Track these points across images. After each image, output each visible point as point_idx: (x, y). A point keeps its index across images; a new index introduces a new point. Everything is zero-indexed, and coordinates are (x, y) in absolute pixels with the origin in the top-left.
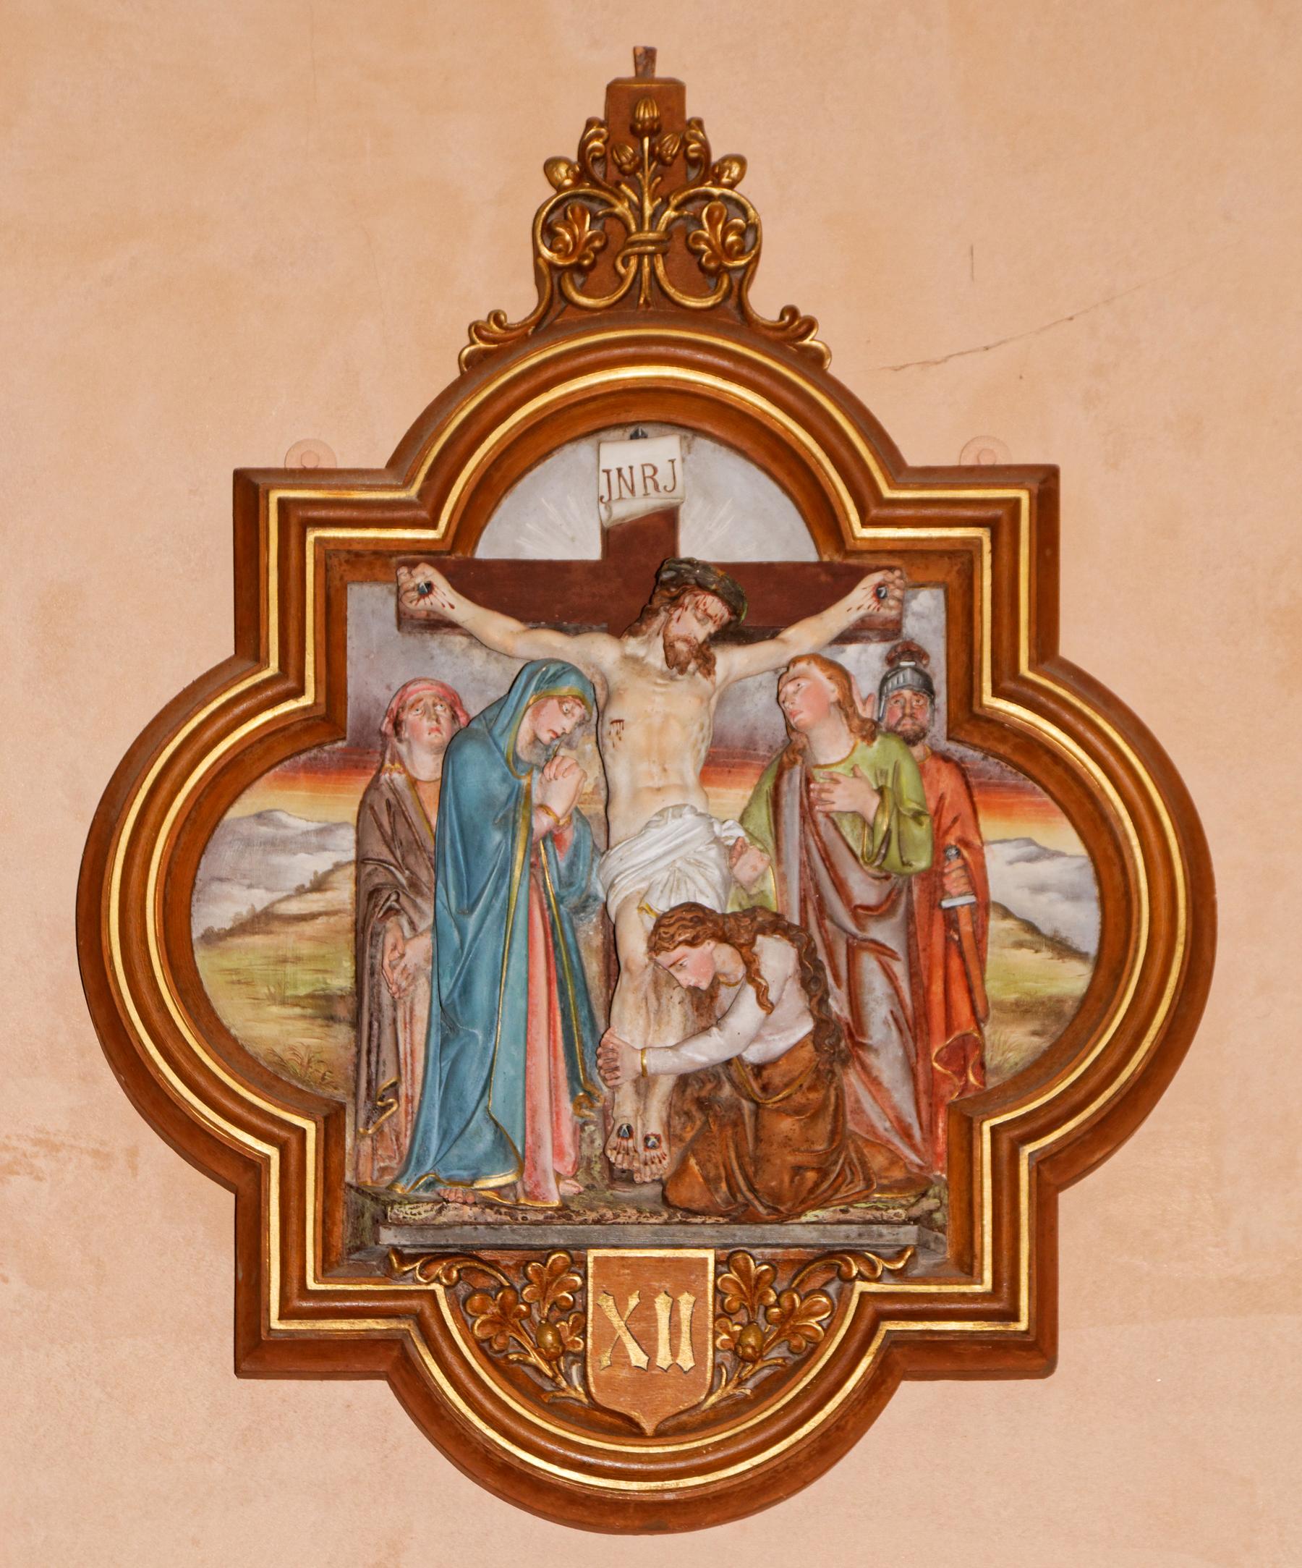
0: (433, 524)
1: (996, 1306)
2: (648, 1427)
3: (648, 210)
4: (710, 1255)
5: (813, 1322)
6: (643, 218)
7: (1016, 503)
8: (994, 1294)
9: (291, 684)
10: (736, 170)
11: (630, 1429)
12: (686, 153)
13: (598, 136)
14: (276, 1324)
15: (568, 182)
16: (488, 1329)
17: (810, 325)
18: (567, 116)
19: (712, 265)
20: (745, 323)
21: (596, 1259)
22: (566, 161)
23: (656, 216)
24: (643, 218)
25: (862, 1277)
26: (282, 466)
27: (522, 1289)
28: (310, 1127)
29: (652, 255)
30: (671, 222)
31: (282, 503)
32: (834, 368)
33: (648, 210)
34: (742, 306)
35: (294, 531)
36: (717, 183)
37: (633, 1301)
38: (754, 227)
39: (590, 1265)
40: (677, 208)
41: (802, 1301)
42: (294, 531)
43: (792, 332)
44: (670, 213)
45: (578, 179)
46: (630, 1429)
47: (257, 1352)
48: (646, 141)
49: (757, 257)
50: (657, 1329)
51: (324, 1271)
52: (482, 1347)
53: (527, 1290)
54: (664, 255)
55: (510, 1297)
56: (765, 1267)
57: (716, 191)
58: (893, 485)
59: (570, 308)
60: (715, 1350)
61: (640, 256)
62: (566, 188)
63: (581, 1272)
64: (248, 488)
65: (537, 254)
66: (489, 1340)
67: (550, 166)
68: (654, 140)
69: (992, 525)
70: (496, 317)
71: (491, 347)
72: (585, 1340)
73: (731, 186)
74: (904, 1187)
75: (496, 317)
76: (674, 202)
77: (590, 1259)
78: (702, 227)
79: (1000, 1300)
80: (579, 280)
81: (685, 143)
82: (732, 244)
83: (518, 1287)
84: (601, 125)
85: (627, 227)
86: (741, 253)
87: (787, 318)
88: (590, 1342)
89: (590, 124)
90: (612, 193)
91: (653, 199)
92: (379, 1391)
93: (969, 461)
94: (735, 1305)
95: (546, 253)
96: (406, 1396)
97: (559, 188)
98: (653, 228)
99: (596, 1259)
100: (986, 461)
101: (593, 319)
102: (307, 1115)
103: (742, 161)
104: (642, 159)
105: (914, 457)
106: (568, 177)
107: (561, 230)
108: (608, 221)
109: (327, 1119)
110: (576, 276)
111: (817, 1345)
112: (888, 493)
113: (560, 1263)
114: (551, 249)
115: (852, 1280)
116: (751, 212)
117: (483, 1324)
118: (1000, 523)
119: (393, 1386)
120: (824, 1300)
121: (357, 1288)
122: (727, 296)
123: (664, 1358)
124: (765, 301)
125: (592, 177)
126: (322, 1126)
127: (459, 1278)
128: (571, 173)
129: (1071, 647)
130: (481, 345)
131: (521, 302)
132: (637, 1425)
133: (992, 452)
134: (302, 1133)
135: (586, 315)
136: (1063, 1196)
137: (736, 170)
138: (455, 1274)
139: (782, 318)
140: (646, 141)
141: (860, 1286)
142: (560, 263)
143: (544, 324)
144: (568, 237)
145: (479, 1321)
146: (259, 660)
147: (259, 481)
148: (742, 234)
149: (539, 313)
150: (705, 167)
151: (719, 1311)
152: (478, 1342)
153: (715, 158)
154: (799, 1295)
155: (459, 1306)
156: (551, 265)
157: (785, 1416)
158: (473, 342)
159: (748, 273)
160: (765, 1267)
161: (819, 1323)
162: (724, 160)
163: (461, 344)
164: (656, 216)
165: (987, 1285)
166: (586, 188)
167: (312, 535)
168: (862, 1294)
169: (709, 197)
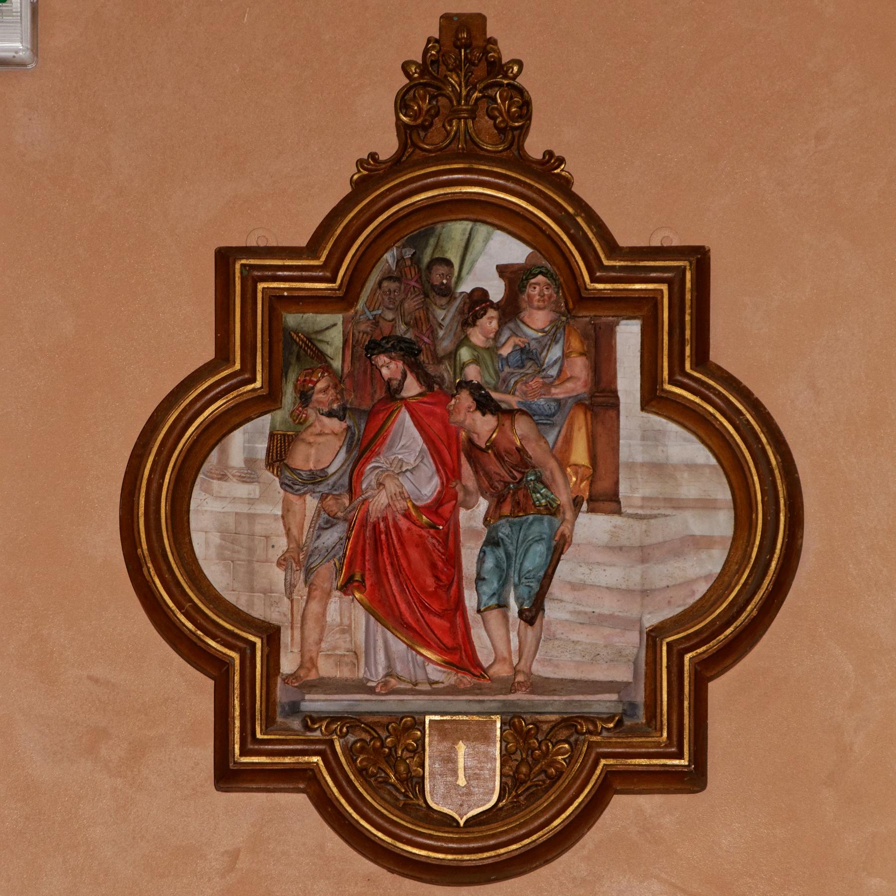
0: (333, 281)
3: (464, 93)
6: (462, 95)
7: (683, 270)
8: (669, 743)
10: (516, 69)
12: (486, 59)
13: (433, 47)
15: (416, 75)
18: (416, 35)
20: (522, 162)
21: (430, 721)
22: (396, 379)
23: (468, 95)
24: (462, 95)
25: (589, 732)
27: (386, 739)
28: (258, 642)
29: (465, 118)
30: (477, 99)
33: (464, 93)
34: (521, 148)
36: (506, 76)
39: (427, 726)
40: (480, 92)
41: (554, 746)
42: (250, 283)
43: (549, 170)
44: (476, 95)
45: (422, 75)
49: (530, 119)
51: (267, 728)
52: (361, 772)
53: (389, 740)
58: (609, 258)
59: (418, 151)
61: (460, 119)
63: (421, 728)
64: (224, 258)
67: (405, 67)
69: (669, 282)
70: (373, 156)
71: (371, 174)
74: (322, 327)
75: (373, 156)
76: (480, 86)
77: (427, 722)
78: (496, 102)
80: (422, 134)
83: (384, 737)
84: (437, 41)
85: (451, 102)
89: (429, 40)
90: (442, 82)
92: (302, 799)
93: (656, 243)
99: (430, 721)
103: (520, 63)
104: (460, 61)
107: (412, 104)
111: (562, 773)
112: (606, 263)
113: (409, 723)
118: (676, 284)
120: (566, 746)
121: (686, 712)
122: (511, 145)
127: (348, 732)
129: (718, 355)
130: (365, 173)
131: (387, 146)
134: (253, 645)
136: (711, 685)
137: (516, 69)
138: (345, 730)
142: (412, 123)
143: (397, 164)
148: (520, 108)
150: (496, 67)
153: (504, 61)
154: (552, 743)
156: (406, 125)
158: (359, 171)
159: (524, 131)
162: (509, 62)
164: (468, 95)
167: (261, 286)
169: (500, 85)
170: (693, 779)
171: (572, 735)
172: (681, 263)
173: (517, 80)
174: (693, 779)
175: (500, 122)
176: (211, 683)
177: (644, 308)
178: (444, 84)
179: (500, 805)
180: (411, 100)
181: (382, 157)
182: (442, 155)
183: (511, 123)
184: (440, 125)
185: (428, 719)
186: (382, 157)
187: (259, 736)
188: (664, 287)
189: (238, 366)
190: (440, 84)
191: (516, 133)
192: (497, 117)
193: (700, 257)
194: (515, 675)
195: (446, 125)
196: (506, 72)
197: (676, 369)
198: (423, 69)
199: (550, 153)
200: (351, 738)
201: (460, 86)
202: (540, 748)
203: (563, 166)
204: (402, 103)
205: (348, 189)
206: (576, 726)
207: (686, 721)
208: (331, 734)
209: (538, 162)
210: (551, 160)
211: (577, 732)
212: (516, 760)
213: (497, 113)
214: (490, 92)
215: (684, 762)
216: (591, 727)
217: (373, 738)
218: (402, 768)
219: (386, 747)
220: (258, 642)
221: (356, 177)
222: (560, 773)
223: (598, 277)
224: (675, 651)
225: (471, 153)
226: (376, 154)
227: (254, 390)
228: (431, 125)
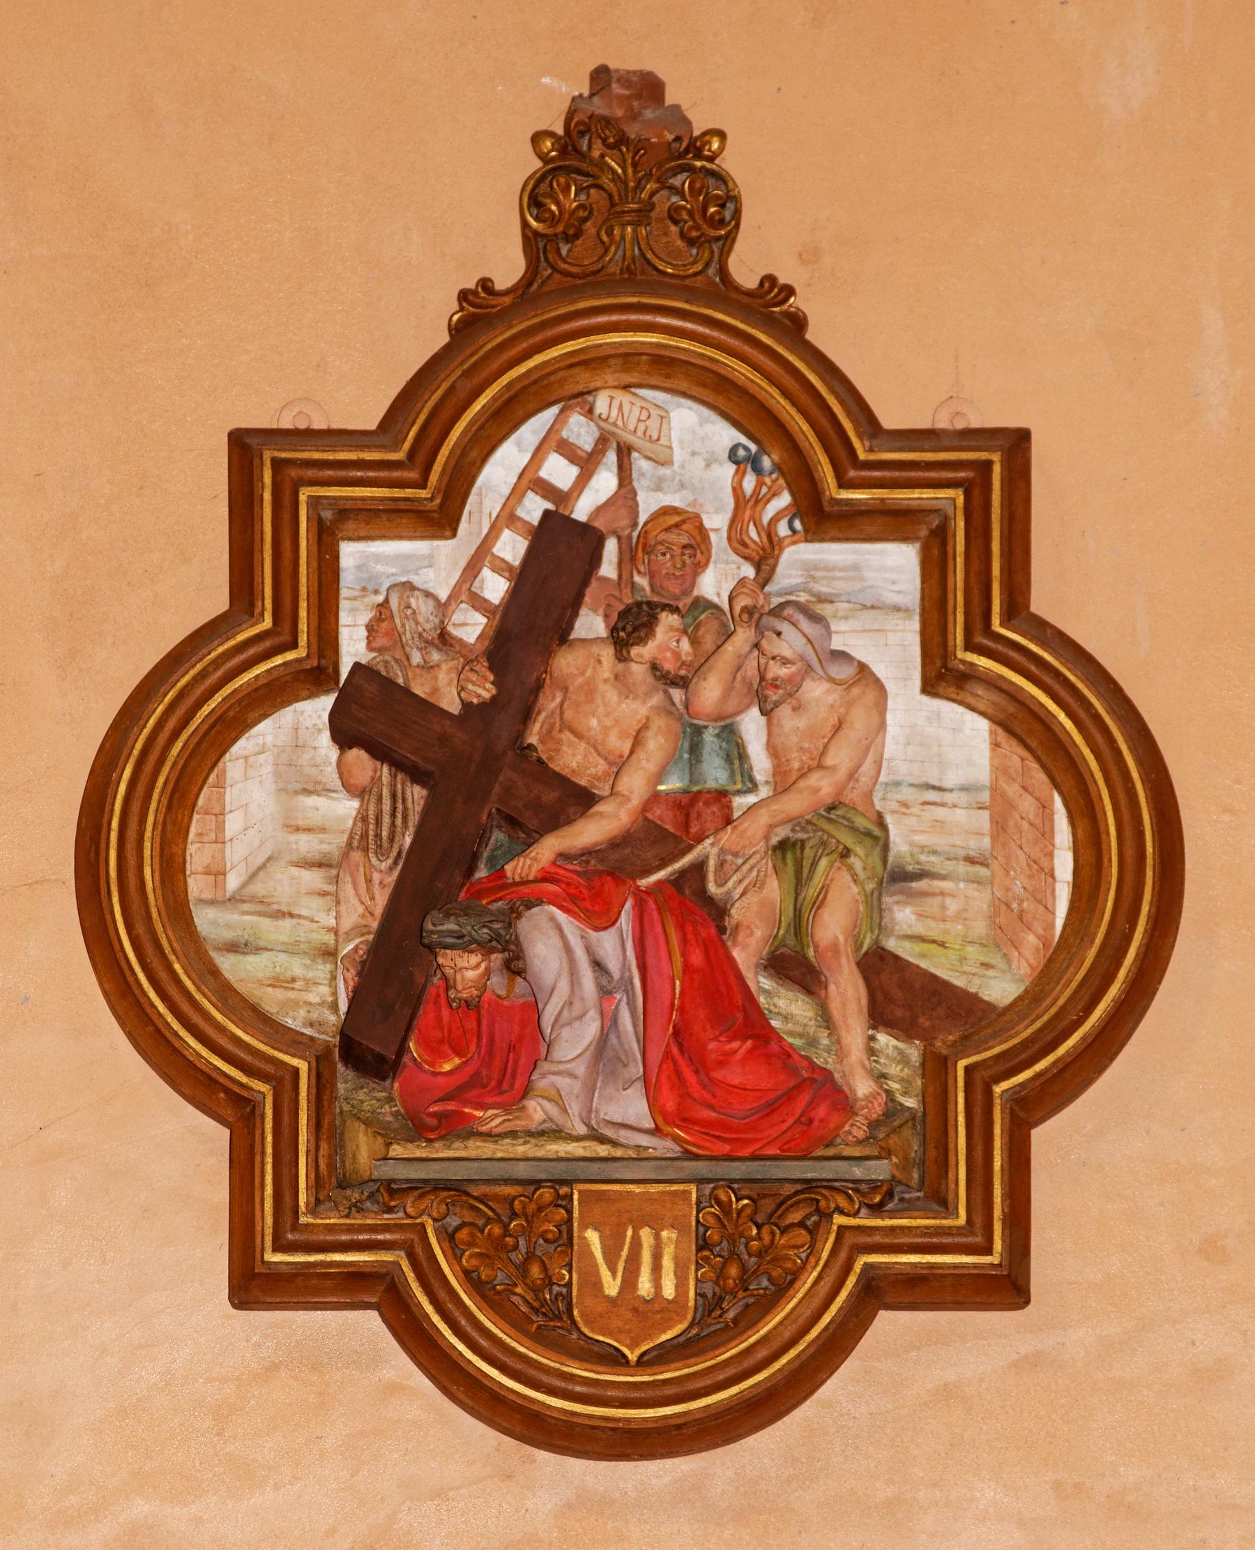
1: (970, 1240)
2: (632, 1356)
6: (627, 223)
9: (285, 638)
10: (715, 146)
11: (616, 1360)
16: (474, 1262)
17: (789, 291)
18: (553, 93)
19: (694, 234)
20: (725, 290)
22: (551, 134)
23: (639, 187)
24: (627, 223)
26: (275, 426)
38: (736, 199)
43: (772, 304)
46: (616, 1360)
47: (252, 1286)
48: (629, 229)
49: (737, 226)
52: (468, 1276)
55: (497, 1230)
56: (746, 1201)
57: (698, 164)
60: (697, 1280)
64: (243, 447)
65: (525, 224)
66: (476, 1270)
70: (485, 284)
71: (479, 310)
72: (570, 1272)
73: (711, 159)
75: (485, 284)
79: (973, 1234)
82: (712, 214)
86: (722, 223)
87: (767, 285)
88: (575, 1276)
92: (370, 1323)
94: (716, 1238)
95: (533, 223)
96: (447, 1384)
97: (542, 157)
101: (574, 287)
103: (722, 135)
105: (888, 421)
108: (592, 191)
109: (318, 1058)
114: (537, 219)
115: (831, 1216)
116: (731, 185)
117: (471, 1256)
118: (976, 486)
119: (381, 1315)
123: (645, 1286)
124: (746, 266)
126: (314, 1064)
128: (556, 146)
129: (1041, 603)
131: (508, 267)
132: (624, 1356)
133: (965, 415)
137: (715, 146)
139: (761, 284)
140: (629, 229)
141: (839, 1220)
143: (525, 291)
144: (554, 208)
145: (467, 1253)
151: (701, 1242)
152: (467, 1273)
155: (448, 1237)
156: (536, 233)
157: (1088, 730)
158: (462, 309)
159: (729, 241)
160: (746, 1201)
161: (738, 1200)
162: (704, 134)
163: (445, 308)
165: (962, 1219)
168: (840, 1227)
170: (1008, 1287)
171: (811, 1214)
172: (983, 455)
173: (717, 161)
174: (1008, 1287)
175: (691, 228)
176: (374, 1314)
178: (602, 170)
180: (546, 195)
181: (501, 284)
182: (594, 280)
184: (593, 231)
186: (501, 284)
189: (268, 623)
190: (591, 169)
191: (716, 247)
192: (686, 222)
193: (1017, 443)
194: (338, 876)
197: (978, 623)
199: (770, 280)
200: (453, 1221)
202: (759, 1237)
203: (792, 299)
204: (535, 197)
205: (445, 338)
206: (818, 1201)
207: (461, 1347)
208: (420, 1215)
209: (749, 294)
210: (774, 291)
211: (818, 1210)
213: (685, 217)
215: (994, 1259)
216: (842, 1202)
217: (489, 1220)
219: (510, 1235)
221: (456, 317)
223: (851, 479)
224: (858, 1267)
225: (639, 274)
226: (490, 280)
227: (298, 661)
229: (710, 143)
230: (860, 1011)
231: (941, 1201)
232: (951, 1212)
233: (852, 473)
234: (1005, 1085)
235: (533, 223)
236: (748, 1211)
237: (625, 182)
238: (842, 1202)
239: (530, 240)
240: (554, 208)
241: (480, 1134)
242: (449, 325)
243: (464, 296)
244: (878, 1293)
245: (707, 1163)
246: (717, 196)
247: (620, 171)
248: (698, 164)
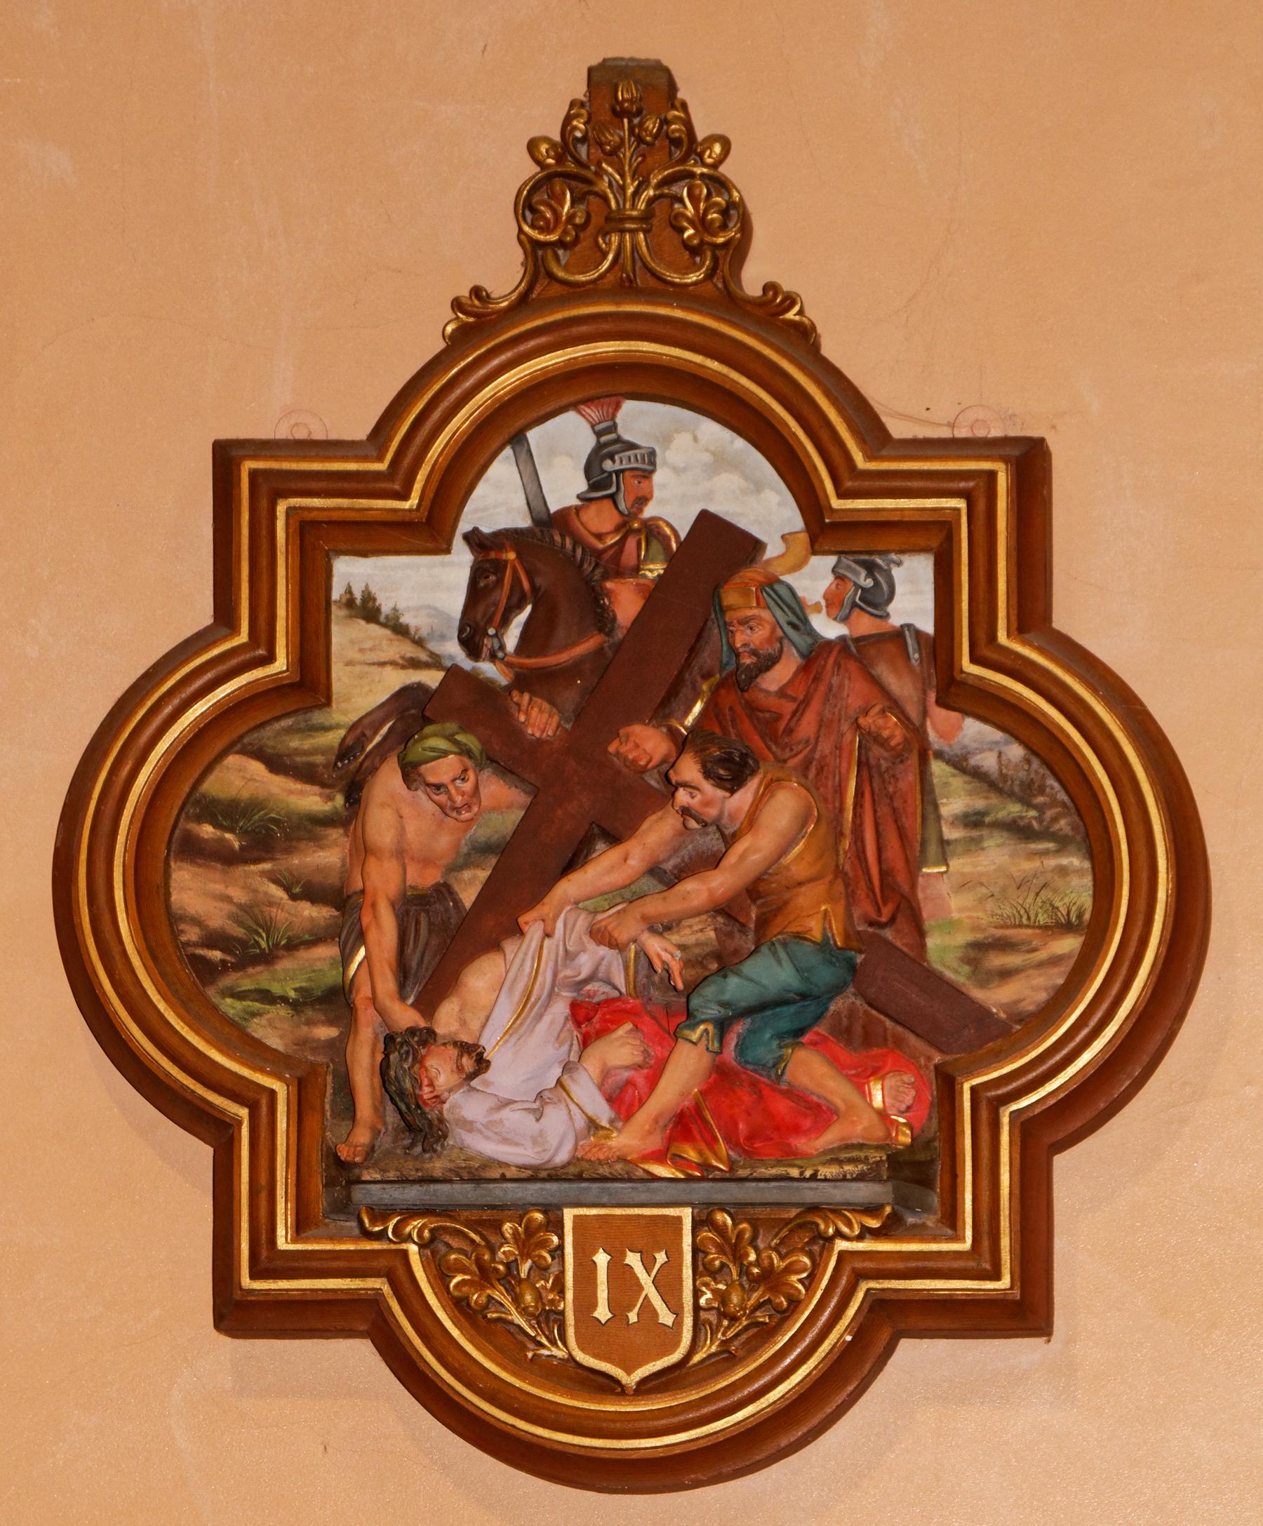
4: (686, 1214)
5: (794, 1278)
6: (630, 223)
14: (246, 1282)
20: (730, 302)
22: (546, 139)
23: (637, 193)
24: (630, 223)
29: (631, 231)
31: (253, 474)
32: (829, 350)
33: (630, 190)
35: (264, 503)
37: (661, 1257)
42: (264, 503)
45: (560, 159)
48: (626, 121)
50: (638, 1289)
52: (459, 1306)
54: (646, 232)
57: (699, 170)
62: (549, 166)
64: (226, 456)
65: (521, 230)
67: (532, 146)
68: (636, 121)
70: (477, 292)
73: (715, 166)
74: (905, 1147)
75: (477, 292)
81: (666, 122)
82: (713, 220)
86: (724, 227)
89: (573, 104)
91: (633, 180)
92: (908, 1349)
95: (526, 229)
98: (633, 207)
100: (981, 433)
102: (279, 1077)
106: (549, 157)
107: (542, 208)
110: (560, 252)
114: (533, 226)
115: (830, 1240)
120: (806, 1260)
124: (753, 279)
125: (562, 176)
129: (1068, 616)
131: (503, 275)
135: (660, 286)
137: (717, 149)
140: (626, 121)
141: (841, 1245)
143: (523, 303)
146: (234, 629)
147: (234, 453)
149: (521, 288)
150: (688, 145)
156: (536, 244)
159: (739, 250)
161: (800, 1281)
162: (705, 140)
164: (637, 193)
165: (967, 1245)
166: (571, 167)
169: (692, 175)
173: (722, 169)
174: (1026, 1313)
177: (936, 537)
179: (697, 1358)
183: (708, 239)
185: (569, 1215)
187: (283, 1243)
188: (961, 504)
192: (685, 229)
193: (1030, 461)
195: (600, 241)
196: (701, 155)
198: (565, 148)
201: (622, 176)
204: (528, 205)
205: (441, 345)
212: (794, 699)
214: (674, 189)
218: (528, 1298)
220: (280, 664)
221: (449, 329)
222: (795, 1303)
228: (577, 240)
229: (711, 149)
230: (373, 1066)
231: (305, 527)
232: (959, 1238)
233: (849, 484)
234: (873, 1284)
235: (526, 229)
236: (747, 1235)
237: (623, 188)
238: (845, 1230)
239: (533, 249)
240: (548, 215)
241: (819, 730)
242: (660, 519)
243: (457, 305)
244: (891, 1320)
245: (711, 1184)
246: (717, 204)
247: (618, 177)
248: (699, 170)
